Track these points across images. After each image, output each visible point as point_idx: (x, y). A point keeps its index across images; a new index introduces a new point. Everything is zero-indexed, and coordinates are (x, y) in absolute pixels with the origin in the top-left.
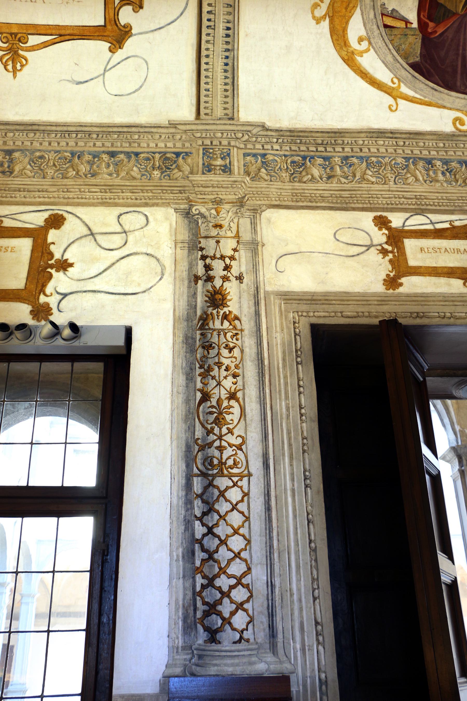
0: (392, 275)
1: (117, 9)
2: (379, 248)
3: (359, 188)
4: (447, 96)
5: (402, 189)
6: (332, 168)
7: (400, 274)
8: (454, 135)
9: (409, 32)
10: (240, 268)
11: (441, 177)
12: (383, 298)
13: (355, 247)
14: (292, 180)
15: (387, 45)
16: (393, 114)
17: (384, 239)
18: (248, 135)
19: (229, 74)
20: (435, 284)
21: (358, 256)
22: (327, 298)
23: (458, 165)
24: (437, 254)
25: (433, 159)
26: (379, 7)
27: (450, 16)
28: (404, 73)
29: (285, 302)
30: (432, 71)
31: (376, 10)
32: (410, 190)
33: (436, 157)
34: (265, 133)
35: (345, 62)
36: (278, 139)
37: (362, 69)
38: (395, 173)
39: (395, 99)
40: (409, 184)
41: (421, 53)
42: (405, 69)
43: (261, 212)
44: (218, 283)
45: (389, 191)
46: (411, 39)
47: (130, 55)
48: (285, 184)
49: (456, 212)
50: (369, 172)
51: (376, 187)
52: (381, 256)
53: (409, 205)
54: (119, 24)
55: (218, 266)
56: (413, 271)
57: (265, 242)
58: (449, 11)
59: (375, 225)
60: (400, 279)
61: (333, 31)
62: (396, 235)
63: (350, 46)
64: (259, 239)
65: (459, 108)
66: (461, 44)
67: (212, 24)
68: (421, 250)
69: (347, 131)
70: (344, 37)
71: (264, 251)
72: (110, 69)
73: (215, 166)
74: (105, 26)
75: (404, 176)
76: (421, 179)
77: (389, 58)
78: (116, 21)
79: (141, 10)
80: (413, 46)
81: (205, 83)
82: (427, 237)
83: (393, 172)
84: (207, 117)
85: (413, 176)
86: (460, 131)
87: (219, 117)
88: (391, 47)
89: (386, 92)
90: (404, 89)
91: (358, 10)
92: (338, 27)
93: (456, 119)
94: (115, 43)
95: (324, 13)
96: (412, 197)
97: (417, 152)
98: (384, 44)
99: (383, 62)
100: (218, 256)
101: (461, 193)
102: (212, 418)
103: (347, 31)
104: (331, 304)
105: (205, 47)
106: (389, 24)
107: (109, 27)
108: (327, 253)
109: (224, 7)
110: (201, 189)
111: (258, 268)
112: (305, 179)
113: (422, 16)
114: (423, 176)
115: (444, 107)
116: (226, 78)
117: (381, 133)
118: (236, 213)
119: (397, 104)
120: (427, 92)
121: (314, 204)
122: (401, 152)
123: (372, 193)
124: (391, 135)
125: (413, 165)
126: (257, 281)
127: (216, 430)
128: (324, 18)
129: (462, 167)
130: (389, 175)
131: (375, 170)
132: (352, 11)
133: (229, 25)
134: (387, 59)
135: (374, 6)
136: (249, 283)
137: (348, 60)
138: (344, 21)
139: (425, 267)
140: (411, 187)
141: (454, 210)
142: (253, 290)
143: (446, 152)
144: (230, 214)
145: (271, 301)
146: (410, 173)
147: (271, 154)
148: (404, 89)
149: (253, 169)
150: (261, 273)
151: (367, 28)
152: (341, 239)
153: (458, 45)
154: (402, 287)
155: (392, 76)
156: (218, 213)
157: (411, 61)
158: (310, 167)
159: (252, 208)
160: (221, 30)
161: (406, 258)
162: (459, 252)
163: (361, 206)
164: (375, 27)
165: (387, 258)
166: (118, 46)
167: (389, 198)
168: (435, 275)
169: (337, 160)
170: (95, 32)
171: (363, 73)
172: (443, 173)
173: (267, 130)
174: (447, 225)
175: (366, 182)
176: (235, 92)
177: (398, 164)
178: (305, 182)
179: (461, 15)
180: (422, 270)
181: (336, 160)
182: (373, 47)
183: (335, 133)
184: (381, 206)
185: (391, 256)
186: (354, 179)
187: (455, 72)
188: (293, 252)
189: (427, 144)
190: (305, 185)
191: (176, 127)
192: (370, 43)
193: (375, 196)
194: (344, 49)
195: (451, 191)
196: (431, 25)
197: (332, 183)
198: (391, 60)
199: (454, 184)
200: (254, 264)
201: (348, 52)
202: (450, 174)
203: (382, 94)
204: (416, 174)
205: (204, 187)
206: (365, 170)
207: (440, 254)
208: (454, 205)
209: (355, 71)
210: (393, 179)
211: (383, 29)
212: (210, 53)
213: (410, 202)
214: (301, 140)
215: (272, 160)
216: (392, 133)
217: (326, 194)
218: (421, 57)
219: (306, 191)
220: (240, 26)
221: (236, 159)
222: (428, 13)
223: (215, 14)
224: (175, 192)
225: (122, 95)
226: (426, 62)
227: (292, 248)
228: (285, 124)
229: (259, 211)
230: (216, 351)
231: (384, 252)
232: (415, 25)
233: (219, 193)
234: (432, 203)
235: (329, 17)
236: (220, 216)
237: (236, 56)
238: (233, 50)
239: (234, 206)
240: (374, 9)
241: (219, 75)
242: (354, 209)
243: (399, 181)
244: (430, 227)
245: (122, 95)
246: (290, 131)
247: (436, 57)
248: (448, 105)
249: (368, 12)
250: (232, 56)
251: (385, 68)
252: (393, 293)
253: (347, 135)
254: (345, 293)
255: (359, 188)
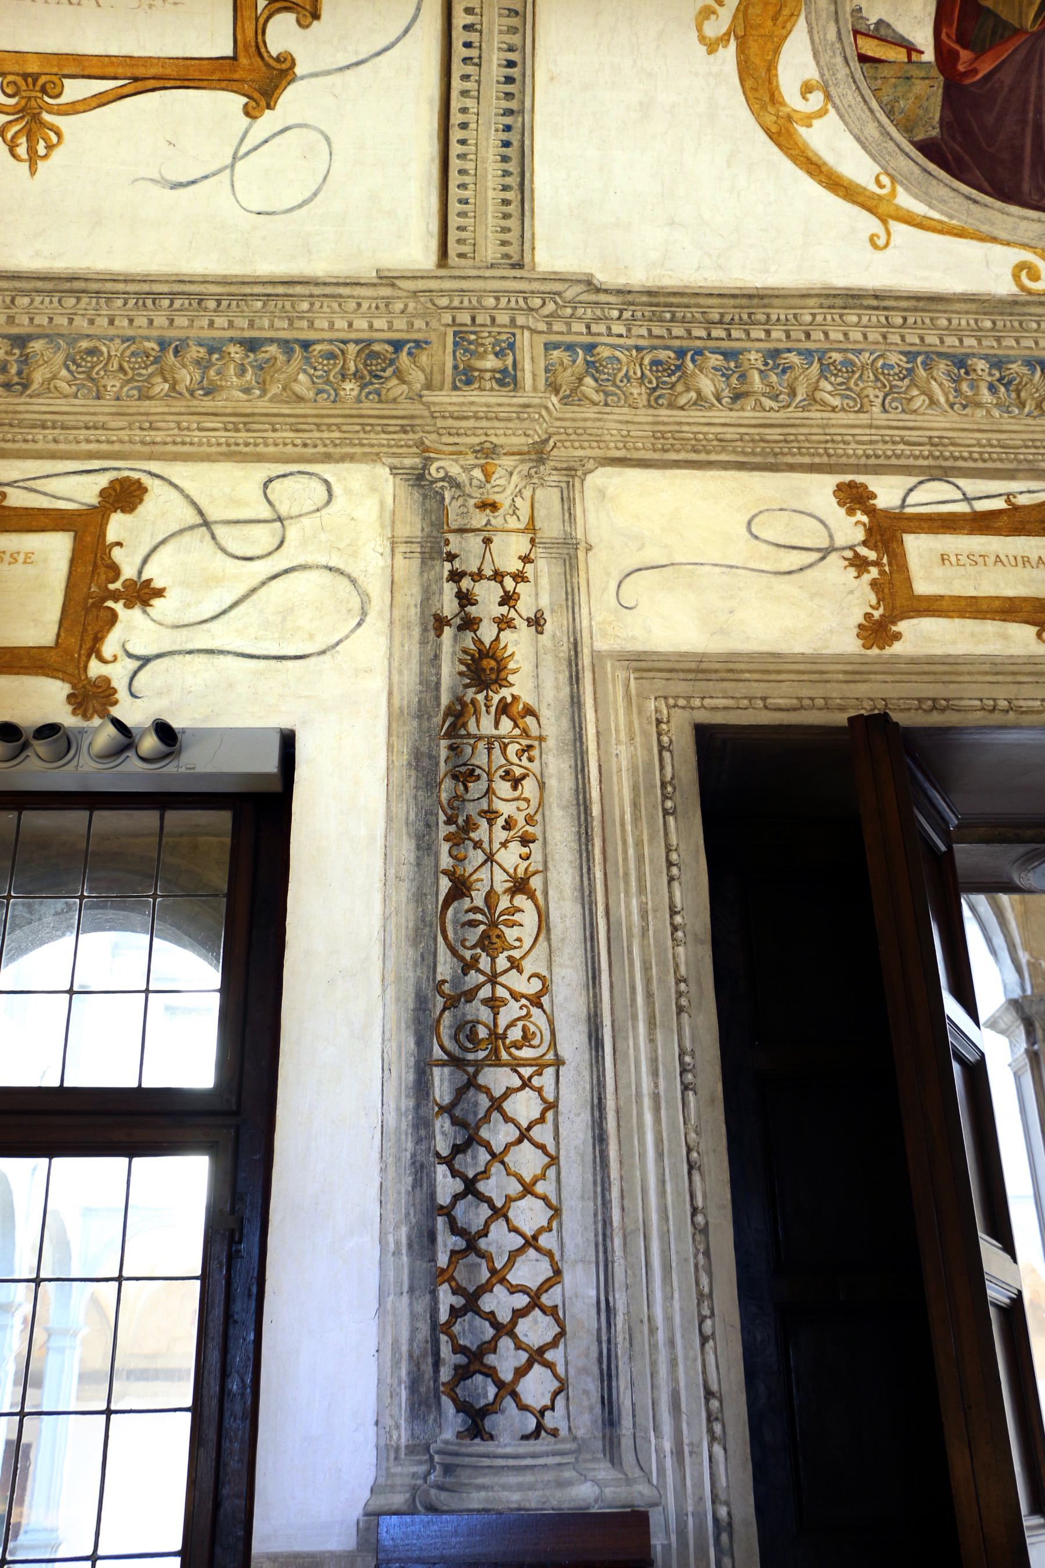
0: (877, 614)
1: (261, 21)
2: (849, 554)
3: (804, 421)
4: (1000, 216)
5: (901, 424)
6: (743, 377)
7: (896, 612)
8: (1015, 303)
9: (915, 72)
10: (537, 599)
11: (986, 396)
12: (857, 667)
13: (795, 552)
14: (653, 403)
15: (865, 101)
16: (879, 255)
17: (860, 535)
18: (555, 302)
19: (512, 167)
20: (973, 635)
21: (802, 574)
22: (731, 666)
23: (1025, 370)
24: (977, 568)
25: (968, 355)
26: (848, 16)
27: (1006, 35)
28: (904, 163)
29: (637, 675)
30: (967, 158)
31: (841, 23)
32: (918, 424)
33: (975, 351)
34: (593, 297)
35: (771, 138)
36: (621, 311)
37: (810, 155)
38: (885, 386)
39: (884, 222)
40: (915, 411)
41: (941, 119)
42: (907, 154)
43: (585, 474)
44: (487, 632)
45: (871, 427)
46: (920, 87)
47: (290, 122)
48: (638, 412)
49: (1020, 475)
50: (825, 385)
51: (842, 418)
52: (852, 572)
53: (916, 458)
54: (265, 55)
55: (487, 594)
56: (925, 605)
57: (592, 541)
58: (1005, 24)
59: (839, 503)
60: (894, 623)
61: (744, 70)
62: (885, 525)
63: (783, 104)
64: (580, 535)
65: (1026, 241)
66: (1032, 98)
67: (473, 53)
68: (943, 560)
69: (776, 293)
70: (770, 83)
71: (591, 561)
72: (247, 154)
73: (480, 371)
74: (235, 58)
75: (905, 393)
76: (942, 400)
77: (871, 130)
78: (259, 48)
79: (315, 23)
80: (925, 104)
81: (459, 187)
82: (955, 529)
83: (879, 385)
84: (463, 262)
85: (923, 393)
86: (1030, 293)
87: (490, 261)
88: (874, 105)
89: (863, 206)
90: (905, 200)
91: (801, 23)
92: (757, 61)
93: (1021, 267)
94: (257, 95)
95: (724, 29)
96: (921, 440)
97: (932, 339)
98: (859, 99)
99: (858, 139)
100: (488, 572)
101: (1032, 432)
102: (474, 935)
103: (776, 69)
104: (741, 681)
105: (460, 106)
106: (870, 53)
107: (243, 60)
108: (732, 567)
109: (500, 15)
110: (450, 422)
111: (576, 601)
112: (682, 401)
113: (944, 37)
114: (946, 394)
115: (994, 240)
116: (506, 173)
117: (853, 296)
118: (529, 476)
119: (889, 234)
120: (956, 206)
121: (703, 457)
122: (897, 339)
123: (833, 431)
124: (874, 303)
125: (925, 370)
126: (574, 628)
127: (484, 963)
128: (724, 39)
129: (1033, 373)
130: (871, 392)
131: (840, 380)
132: (789, 25)
133: (512, 56)
134: (866, 133)
135: (836, 12)
136: (558, 634)
137: (779, 133)
138: (770, 46)
139: (950, 597)
140: (919, 418)
141: (1017, 470)
142: (565, 648)
143: (998, 339)
144: (515, 478)
145: (606, 673)
146: (917, 386)
147: (606, 345)
148: (905, 200)
149: (566, 378)
150: (585, 611)
151: (822, 62)
152: (762, 535)
153: (1025, 101)
154: (901, 642)
155: (878, 170)
156: (488, 476)
157: (920, 137)
158: (693, 375)
159: (565, 465)
160: (495, 67)
161: (909, 578)
162: (1027, 565)
163: (807, 460)
164: (839, 60)
165: (867, 578)
166: (263, 103)
167: (871, 442)
168: (974, 615)
169: (754, 357)
170: (213, 73)
171: (812, 163)
172: (992, 388)
173: (598, 290)
174: (999, 504)
175: (819, 407)
176: (526, 207)
177: (892, 367)
178: (682, 408)
179: (1033, 34)
180: (944, 603)
181: (752, 357)
182: (835, 106)
183: (750, 297)
184: (853, 461)
185: (874, 572)
186: (792, 400)
187: (1017, 160)
188: (655, 564)
189: (955, 322)
190: (682, 413)
191: (393, 285)
192: (828, 97)
193: (839, 438)
194: (770, 109)
195: (1009, 428)
196: (965, 55)
197: (743, 409)
198: (876, 134)
199: (1017, 411)
200: (569, 590)
201: (778, 117)
202: (1007, 390)
203: (856, 210)
204: (930, 390)
205: (458, 418)
206: (818, 381)
207: (984, 568)
208: (1015, 459)
209: (794, 159)
210: (880, 400)
211: (858, 65)
212: (471, 118)
213: (917, 451)
214: (673, 314)
215: (609, 358)
216: (876, 297)
217: (730, 433)
218: (941, 127)
219: (685, 428)
220: (537, 59)
221: (527, 356)
222: (957, 30)
223: (481, 32)
224: (391, 429)
225: (273, 213)
226: (954, 138)
227: (652, 555)
228: (638, 277)
229: (579, 473)
230: (483, 785)
231: (860, 564)
232: (929, 56)
233: (489, 432)
234: (966, 455)
235: (737, 38)
236: (493, 483)
237: (527, 126)
238: (522, 111)
239: (523, 461)
240: (837, 21)
241: (490, 169)
242: (792, 468)
243: (894, 405)
244: (963, 508)
245: (273, 213)
246: (650, 293)
247: (976, 128)
248: (1003, 235)
249: (824, 28)
250: (519, 125)
251: (862, 152)
252: (879, 656)
253: (777, 302)
254: (772, 654)
255: (804, 421)
